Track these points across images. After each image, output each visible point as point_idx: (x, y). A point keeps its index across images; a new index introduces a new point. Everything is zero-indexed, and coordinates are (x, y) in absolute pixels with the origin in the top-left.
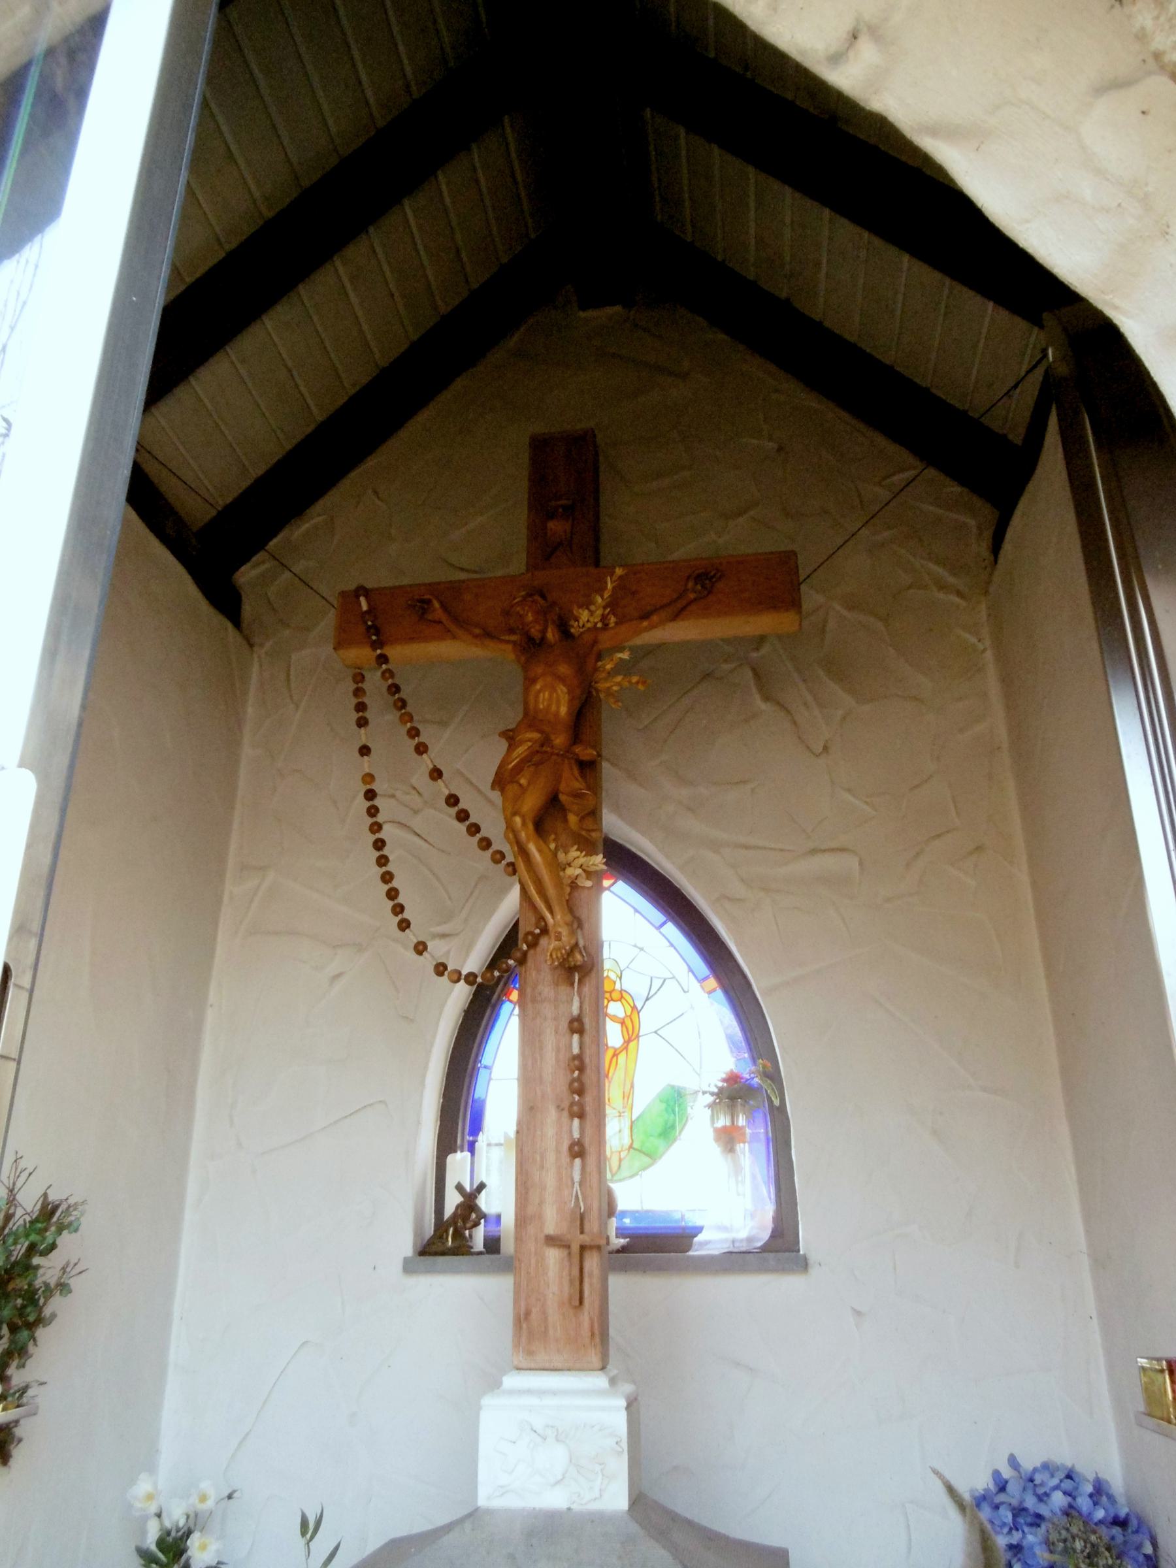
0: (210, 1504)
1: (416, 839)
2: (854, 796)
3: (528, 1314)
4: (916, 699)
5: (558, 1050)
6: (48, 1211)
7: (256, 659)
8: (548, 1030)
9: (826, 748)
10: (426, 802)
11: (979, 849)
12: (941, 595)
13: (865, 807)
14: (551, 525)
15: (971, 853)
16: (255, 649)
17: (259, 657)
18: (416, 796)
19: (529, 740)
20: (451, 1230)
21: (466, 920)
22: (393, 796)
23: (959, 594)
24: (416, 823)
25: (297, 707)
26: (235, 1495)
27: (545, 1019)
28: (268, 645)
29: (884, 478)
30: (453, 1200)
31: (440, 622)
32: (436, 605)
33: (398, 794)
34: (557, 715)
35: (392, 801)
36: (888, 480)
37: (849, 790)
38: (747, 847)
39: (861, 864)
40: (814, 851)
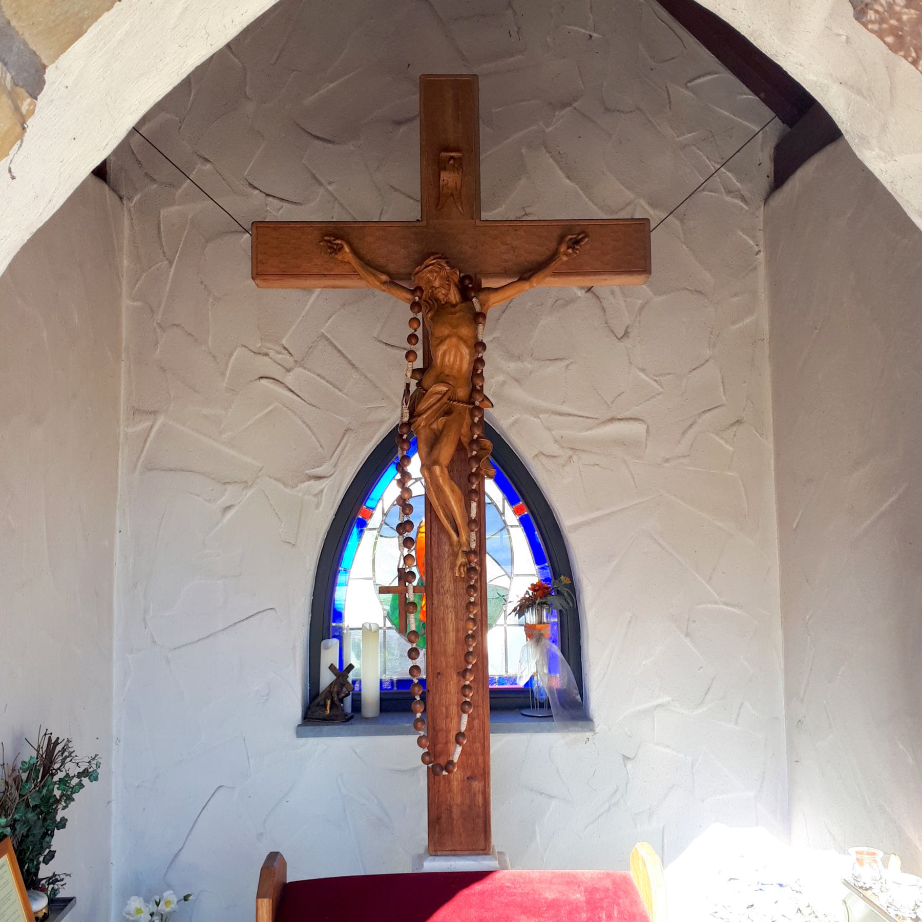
0: (173, 906)
1: (291, 394)
2: (646, 375)
3: (439, 818)
4: (700, 292)
5: (457, 631)
6: (52, 745)
7: (126, 213)
8: (450, 616)
9: (626, 333)
10: (296, 361)
11: (739, 422)
12: (728, 198)
13: (654, 384)
14: (444, 176)
15: (732, 425)
16: (125, 202)
17: (129, 211)
18: (288, 357)
19: (438, 393)
20: (329, 702)
21: (335, 466)
22: (266, 355)
23: (743, 198)
24: (289, 379)
25: (171, 263)
26: (190, 898)
27: (447, 608)
28: (136, 198)
29: (690, 81)
30: (327, 678)
31: (349, 263)
32: (347, 249)
33: (272, 353)
34: (460, 370)
35: (266, 359)
36: (693, 83)
37: (643, 370)
38: (561, 414)
39: (647, 431)
40: (612, 420)
